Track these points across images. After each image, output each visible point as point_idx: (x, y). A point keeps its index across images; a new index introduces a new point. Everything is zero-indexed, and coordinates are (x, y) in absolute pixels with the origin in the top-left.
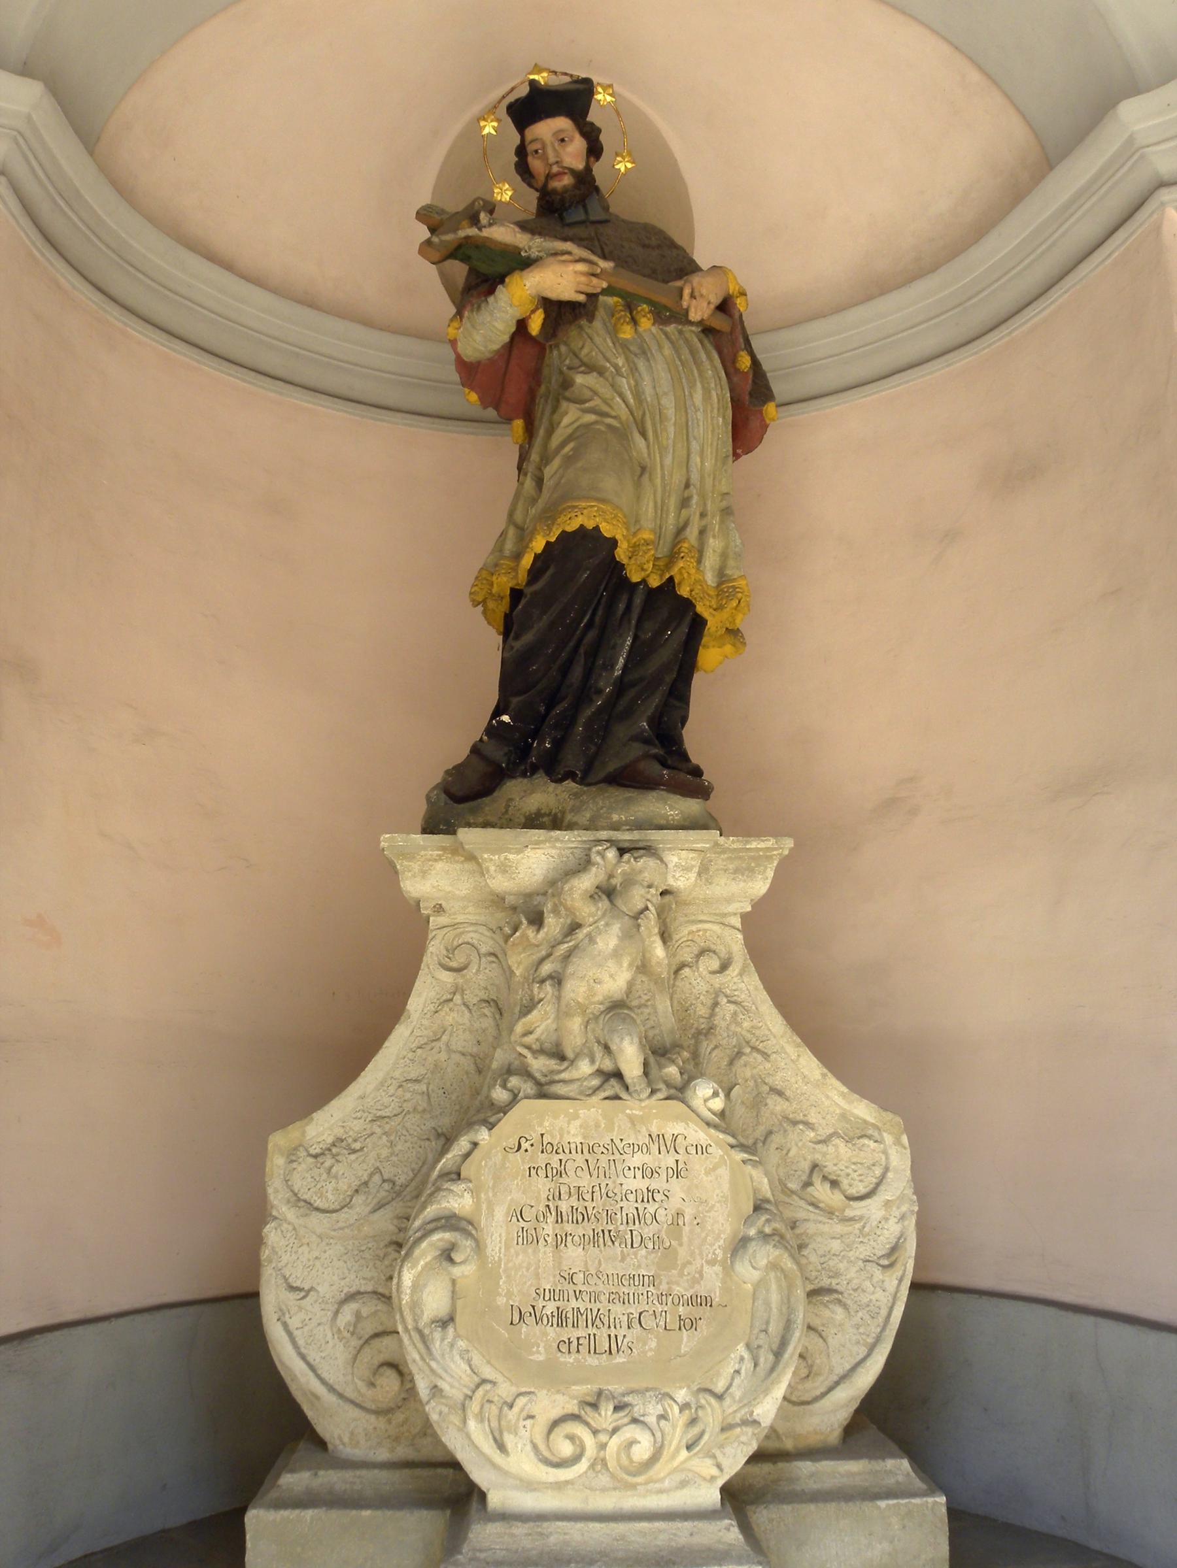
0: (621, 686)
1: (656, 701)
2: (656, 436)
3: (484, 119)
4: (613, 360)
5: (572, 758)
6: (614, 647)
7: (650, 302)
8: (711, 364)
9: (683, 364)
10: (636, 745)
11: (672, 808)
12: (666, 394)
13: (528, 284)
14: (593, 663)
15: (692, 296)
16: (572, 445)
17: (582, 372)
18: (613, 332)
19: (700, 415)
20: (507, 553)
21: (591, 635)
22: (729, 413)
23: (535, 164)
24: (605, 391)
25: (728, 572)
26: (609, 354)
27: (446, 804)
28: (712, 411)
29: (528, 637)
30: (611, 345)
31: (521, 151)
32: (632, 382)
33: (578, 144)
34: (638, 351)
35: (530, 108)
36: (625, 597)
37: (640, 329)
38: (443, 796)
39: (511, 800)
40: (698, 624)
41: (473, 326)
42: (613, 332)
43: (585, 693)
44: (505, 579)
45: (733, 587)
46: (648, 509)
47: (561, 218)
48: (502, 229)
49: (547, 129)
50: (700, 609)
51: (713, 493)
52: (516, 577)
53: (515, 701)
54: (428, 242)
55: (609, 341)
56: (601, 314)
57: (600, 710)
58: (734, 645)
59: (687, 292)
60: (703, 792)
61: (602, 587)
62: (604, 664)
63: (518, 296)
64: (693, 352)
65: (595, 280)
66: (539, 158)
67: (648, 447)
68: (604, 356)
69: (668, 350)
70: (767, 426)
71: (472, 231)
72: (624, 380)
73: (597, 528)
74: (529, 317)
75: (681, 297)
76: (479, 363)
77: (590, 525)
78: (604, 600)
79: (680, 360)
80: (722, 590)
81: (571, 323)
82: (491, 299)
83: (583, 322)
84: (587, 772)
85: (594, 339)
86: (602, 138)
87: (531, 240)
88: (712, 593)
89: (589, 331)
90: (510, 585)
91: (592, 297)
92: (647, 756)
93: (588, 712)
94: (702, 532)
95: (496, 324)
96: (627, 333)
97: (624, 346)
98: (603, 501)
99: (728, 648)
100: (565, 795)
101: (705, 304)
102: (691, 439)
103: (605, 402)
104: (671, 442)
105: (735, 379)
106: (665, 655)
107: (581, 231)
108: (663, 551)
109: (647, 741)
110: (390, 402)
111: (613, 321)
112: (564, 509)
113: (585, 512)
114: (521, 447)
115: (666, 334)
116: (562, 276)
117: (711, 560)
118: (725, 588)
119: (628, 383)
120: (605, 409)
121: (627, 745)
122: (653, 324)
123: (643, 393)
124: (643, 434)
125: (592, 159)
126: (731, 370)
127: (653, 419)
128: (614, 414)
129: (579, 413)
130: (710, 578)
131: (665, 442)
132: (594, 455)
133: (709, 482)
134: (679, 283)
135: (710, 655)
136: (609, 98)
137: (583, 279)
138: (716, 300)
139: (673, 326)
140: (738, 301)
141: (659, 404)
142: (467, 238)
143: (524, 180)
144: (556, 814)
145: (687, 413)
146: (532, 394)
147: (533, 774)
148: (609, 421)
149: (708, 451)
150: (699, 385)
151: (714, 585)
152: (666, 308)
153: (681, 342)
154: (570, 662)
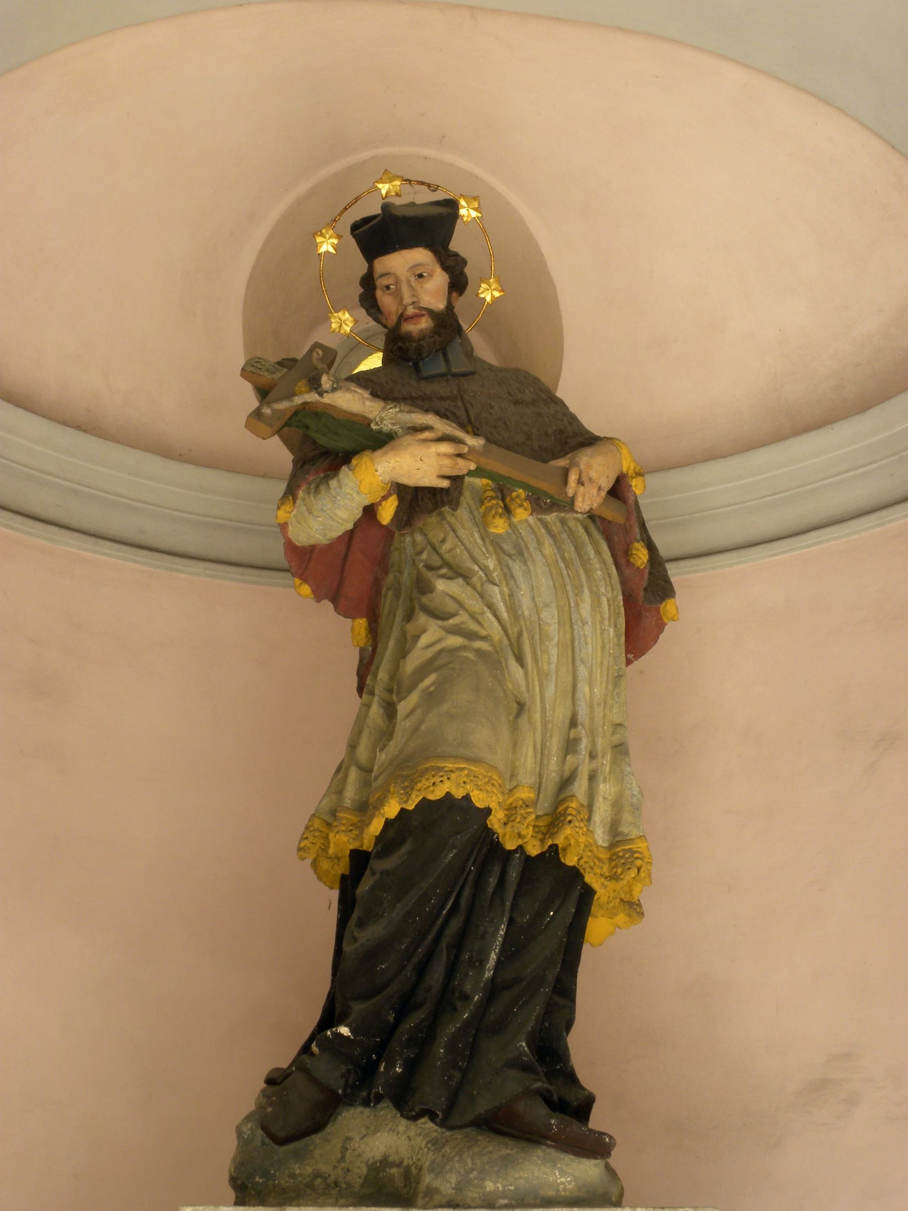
0: (494, 990)
1: (536, 1009)
2: (536, 660)
3: (322, 235)
4: (482, 560)
5: (431, 1090)
6: (483, 937)
7: (526, 487)
8: (599, 558)
9: (567, 567)
10: (513, 1073)
11: (563, 1173)
12: (547, 605)
13: (380, 470)
14: (457, 956)
15: (580, 482)
16: (432, 678)
17: (443, 576)
18: (482, 525)
19: (588, 630)
20: (348, 803)
21: (456, 924)
22: (622, 620)
23: (385, 300)
24: (474, 603)
25: (624, 829)
26: (476, 553)
27: (263, 1143)
28: (602, 622)
29: (376, 931)
30: (479, 541)
31: (368, 282)
32: (506, 590)
33: (439, 279)
34: (513, 551)
35: (380, 234)
36: (496, 870)
37: (515, 520)
38: (260, 1132)
39: (349, 1139)
40: (588, 893)
41: (310, 512)
42: (482, 525)
43: (447, 1001)
44: (345, 839)
45: (630, 850)
46: (527, 759)
47: (417, 369)
48: (348, 396)
49: (401, 263)
50: (589, 879)
51: (603, 725)
52: (360, 837)
53: (358, 1008)
54: (257, 414)
55: (476, 535)
56: (467, 498)
57: (466, 1024)
58: (629, 915)
59: (573, 477)
60: (597, 1147)
61: (471, 862)
62: (470, 958)
63: (369, 480)
64: (578, 548)
65: (461, 462)
66: (390, 294)
67: (526, 674)
68: (471, 556)
69: (549, 548)
70: (664, 625)
71: (312, 397)
72: (496, 589)
73: (467, 798)
74: (379, 503)
75: (566, 482)
76: (313, 548)
77: (459, 794)
78: (471, 877)
79: (564, 559)
80: (616, 854)
81: (430, 512)
82: (333, 483)
83: (446, 509)
84: (448, 1112)
85: (459, 533)
86: (467, 270)
87: (384, 408)
88: (604, 855)
89: (452, 520)
90: (352, 847)
91: (456, 480)
92: (529, 1093)
93: (452, 1028)
94: (592, 777)
95: (338, 512)
96: (499, 526)
97: (496, 544)
98: (476, 761)
99: (621, 918)
100: (420, 1142)
101: (594, 491)
102: (578, 663)
103: (472, 616)
104: (553, 666)
105: (627, 572)
106: (545, 946)
107: (440, 388)
108: (545, 805)
109: (526, 1068)
110: (191, 549)
111: (482, 510)
112: (427, 770)
113: (453, 776)
114: (362, 650)
115: (546, 525)
116: (420, 462)
117: (602, 812)
118: (622, 853)
119: (501, 592)
120: (473, 626)
121: (503, 1083)
122: (531, 514)
123: (520, 606)
124: (520, 660)
125: (455, 294)
126: (623, 561)
127: (532, 638)
128: (483, 633)
129: (442, 633)
130: (601, 837)
131: (545, 667)
132: (461, 696)
133: (599, 712)
134: (562, 463)
135: (598, 926)
136: (474, 214)
137: (447, 462)
138: (607, 485)
139: (554, 515)
140: (634, 483)
141: (539, 618)
142: (305, 404)
143: (369, 314)
144: (408, 1167)
145: (571, 626)
146: (377, 585)
147: (376, 1104)
148: (479, 644)
149: (597, 673)
150: (586, 591)
151: (606, 845)
152: (547, 495)
153: (565, 536)
154: (429, 957)
